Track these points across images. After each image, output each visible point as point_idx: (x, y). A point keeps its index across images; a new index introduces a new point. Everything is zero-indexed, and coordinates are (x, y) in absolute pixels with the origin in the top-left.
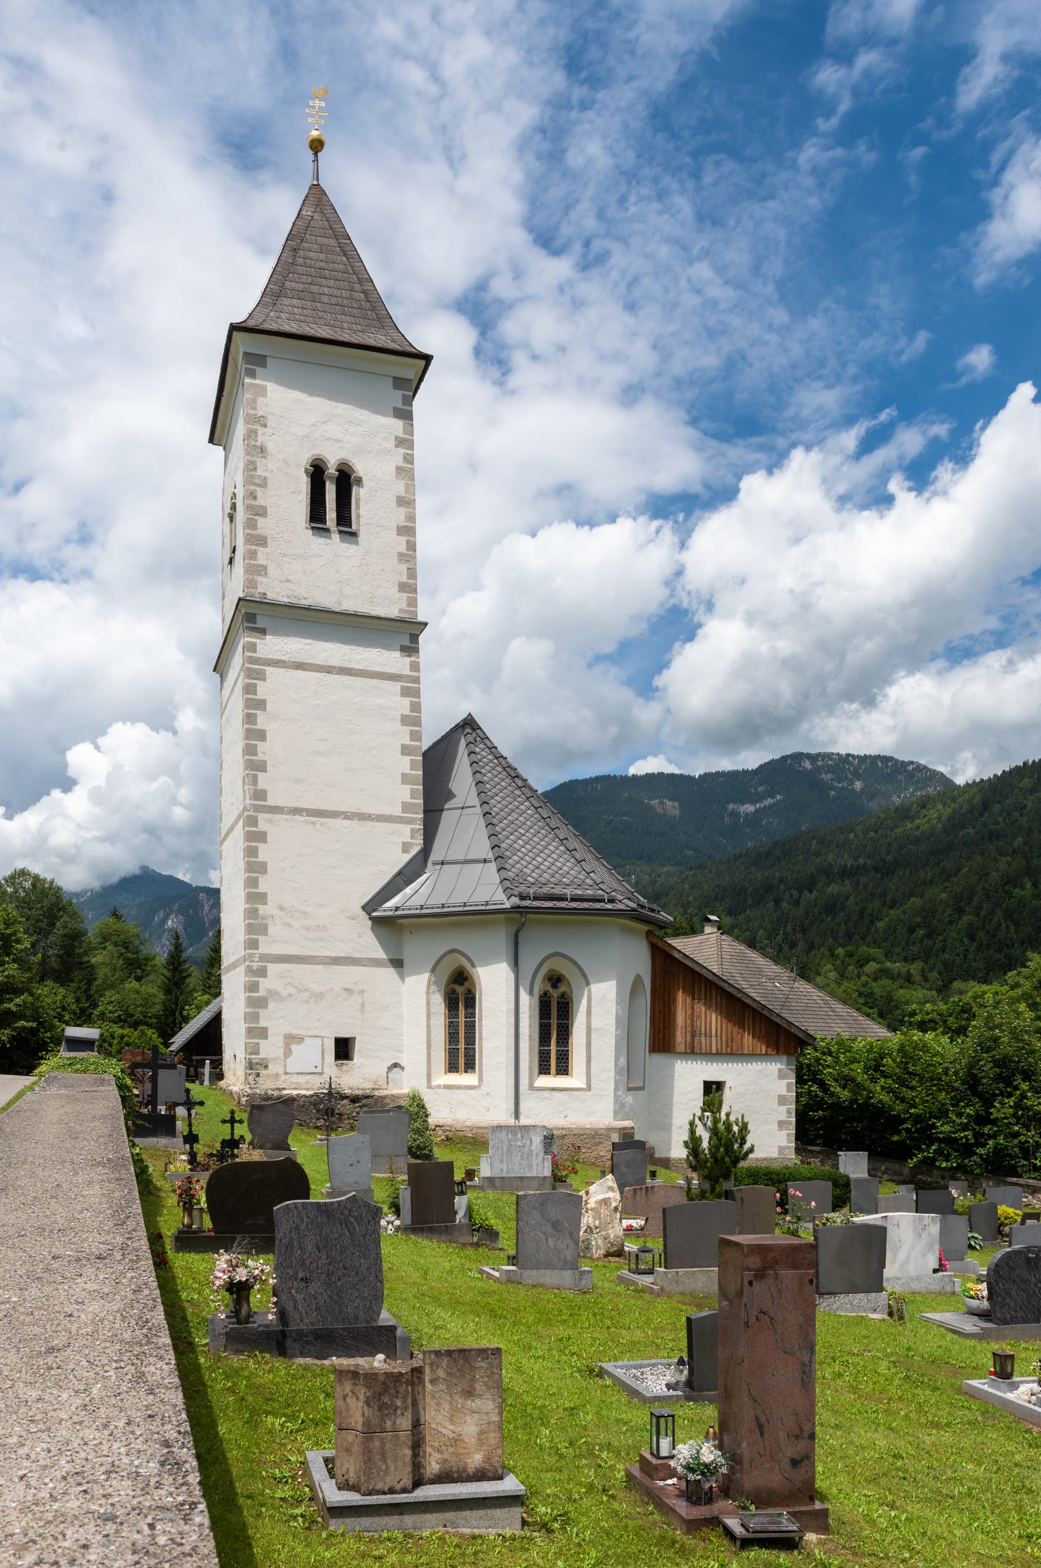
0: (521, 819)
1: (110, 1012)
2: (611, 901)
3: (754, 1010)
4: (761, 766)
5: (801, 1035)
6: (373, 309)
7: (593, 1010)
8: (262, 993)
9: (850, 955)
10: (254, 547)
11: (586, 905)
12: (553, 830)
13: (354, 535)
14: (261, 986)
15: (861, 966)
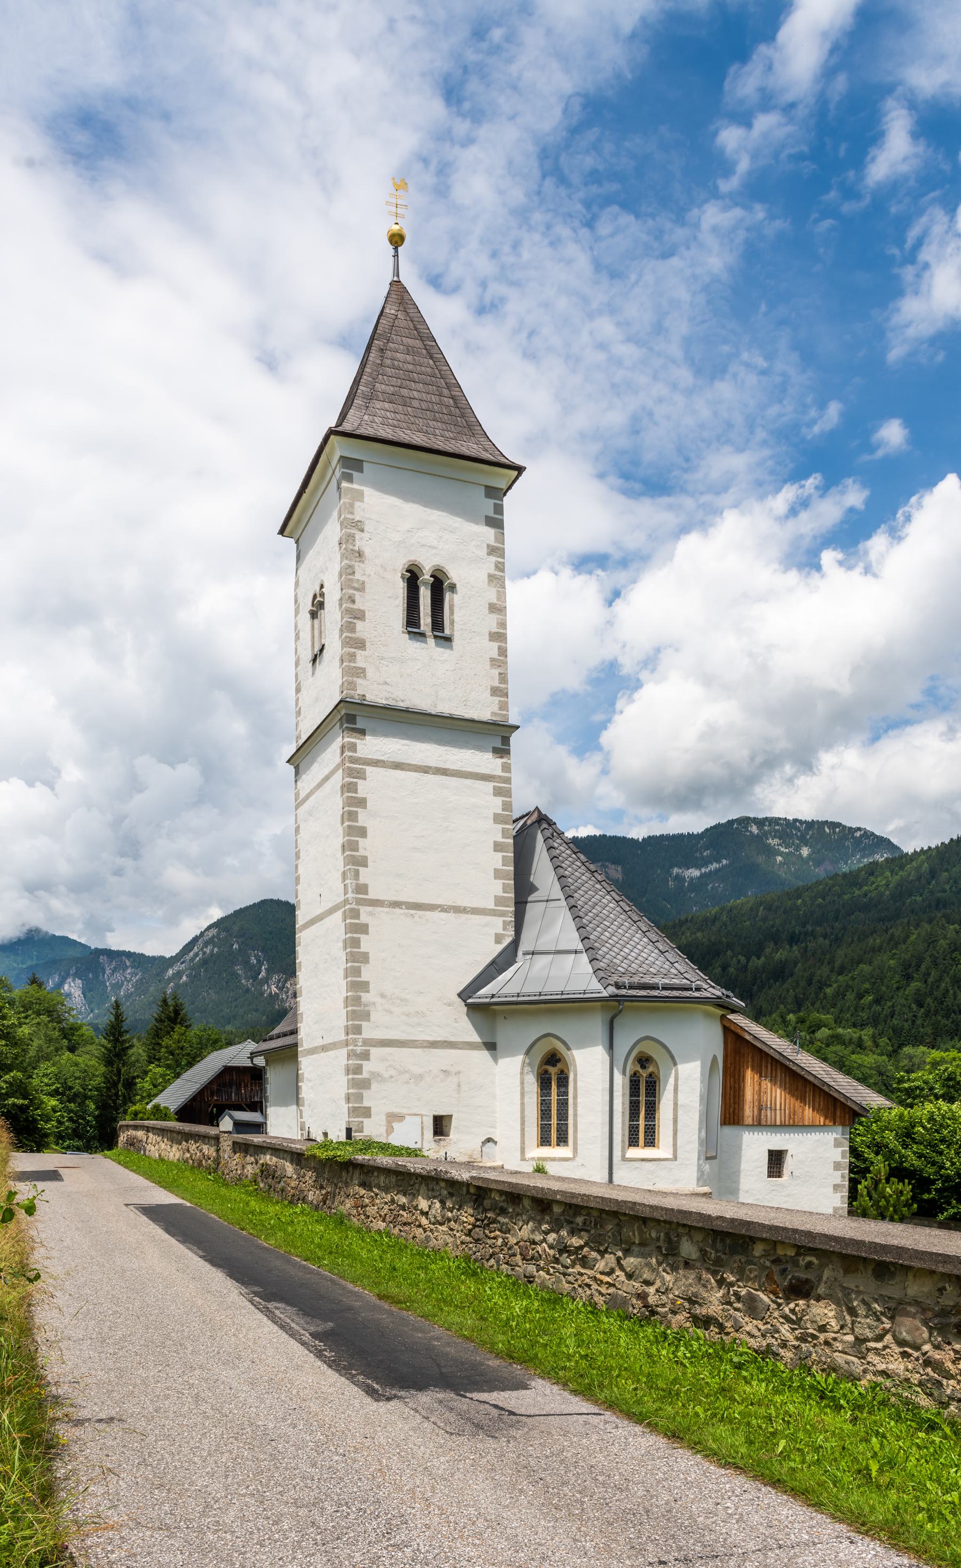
0: (604, 911)
1: (47, 1085)
2: (698, 989)
3: (814, 1085)
4: (707, 830)
5: (856, 1108)
6: (463, 416)
7: (679, 1089)
8: (365, 1075)
9: (802, 1021)
10: (353, 650)
11: (676, 993)
12: (635, 922)
13: (448, 639)
14: (365, 1069)
15: (813, 1032)
